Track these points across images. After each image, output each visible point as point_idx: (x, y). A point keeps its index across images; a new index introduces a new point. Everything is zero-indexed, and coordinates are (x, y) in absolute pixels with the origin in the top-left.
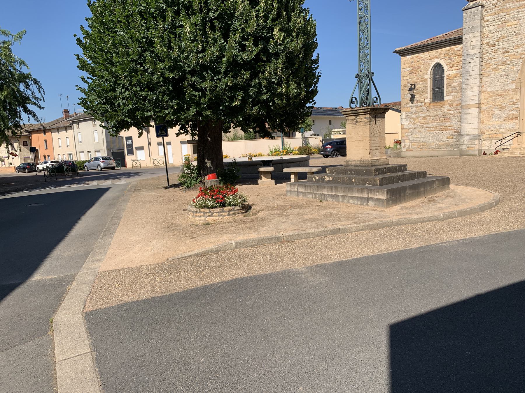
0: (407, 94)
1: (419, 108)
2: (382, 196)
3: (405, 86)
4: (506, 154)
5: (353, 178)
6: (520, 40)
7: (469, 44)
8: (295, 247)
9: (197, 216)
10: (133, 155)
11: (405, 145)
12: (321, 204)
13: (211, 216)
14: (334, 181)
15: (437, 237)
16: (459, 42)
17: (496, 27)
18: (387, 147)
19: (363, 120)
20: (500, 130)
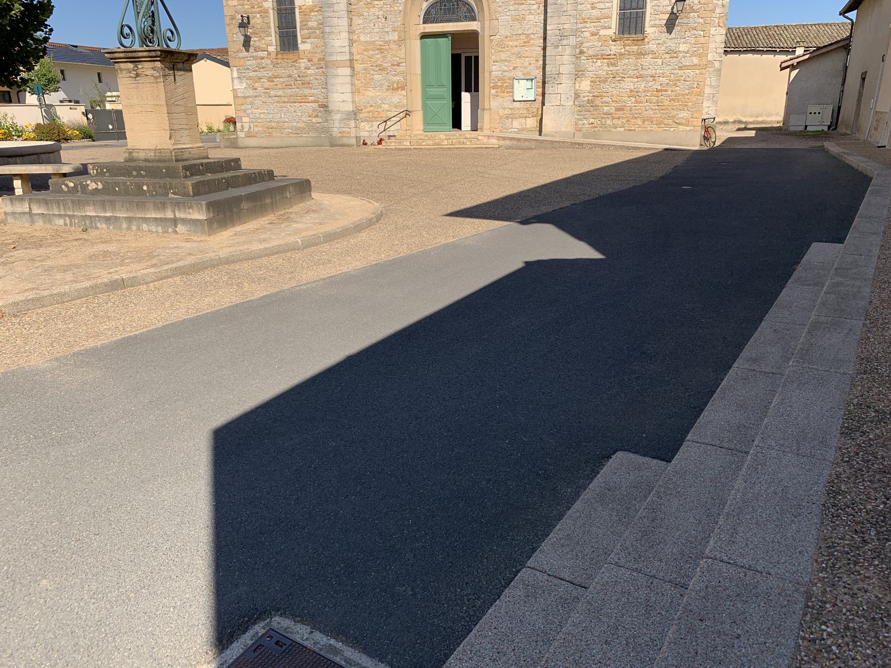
0: (236, 34)
1: (260, 61)
4: (392, 144)
8: (29, 324)
11: (242, 126)
12: (85, 236)
14: (108, 190)
15: (293, 277)
18: (215, 131)
19: (149, 72)
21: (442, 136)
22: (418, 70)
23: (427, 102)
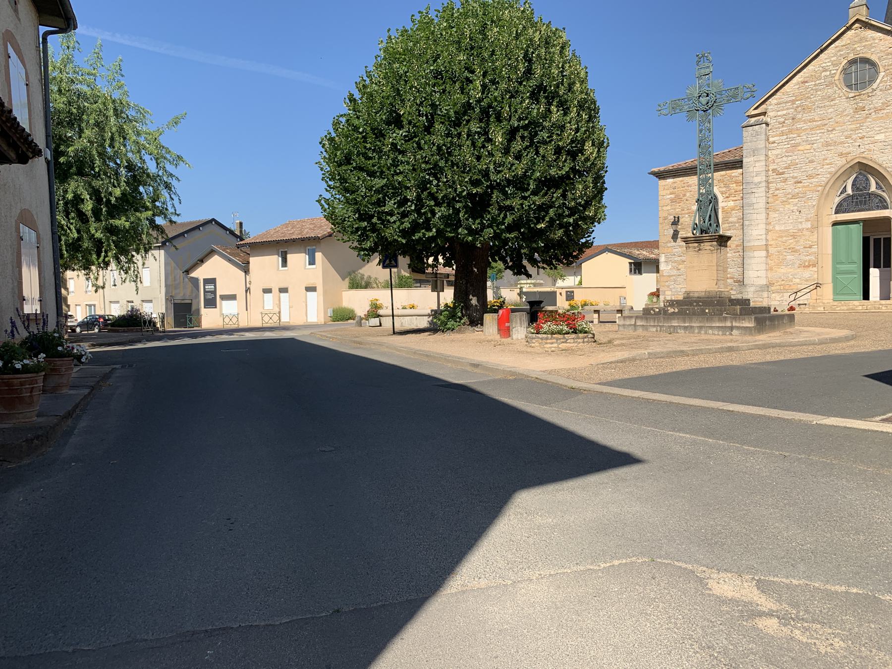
2: (751, 324)
3: (665, 218)
5: (706, 309)
6: (815, 168)
7: (751, 169)
9: (546, 343)
10: (216, 307)
13: (566, 342)
16: (738, 166)
17: (784, 151)
20: (794, 280)
21: (856, 303)
22: (830, 251)
23: (838, 276)
